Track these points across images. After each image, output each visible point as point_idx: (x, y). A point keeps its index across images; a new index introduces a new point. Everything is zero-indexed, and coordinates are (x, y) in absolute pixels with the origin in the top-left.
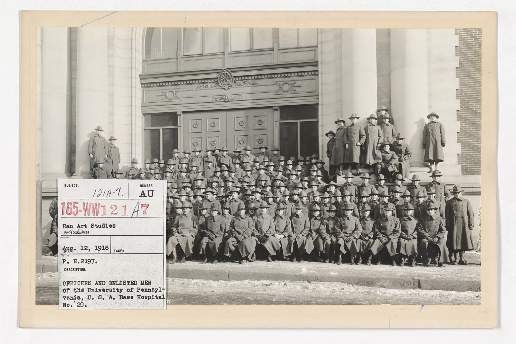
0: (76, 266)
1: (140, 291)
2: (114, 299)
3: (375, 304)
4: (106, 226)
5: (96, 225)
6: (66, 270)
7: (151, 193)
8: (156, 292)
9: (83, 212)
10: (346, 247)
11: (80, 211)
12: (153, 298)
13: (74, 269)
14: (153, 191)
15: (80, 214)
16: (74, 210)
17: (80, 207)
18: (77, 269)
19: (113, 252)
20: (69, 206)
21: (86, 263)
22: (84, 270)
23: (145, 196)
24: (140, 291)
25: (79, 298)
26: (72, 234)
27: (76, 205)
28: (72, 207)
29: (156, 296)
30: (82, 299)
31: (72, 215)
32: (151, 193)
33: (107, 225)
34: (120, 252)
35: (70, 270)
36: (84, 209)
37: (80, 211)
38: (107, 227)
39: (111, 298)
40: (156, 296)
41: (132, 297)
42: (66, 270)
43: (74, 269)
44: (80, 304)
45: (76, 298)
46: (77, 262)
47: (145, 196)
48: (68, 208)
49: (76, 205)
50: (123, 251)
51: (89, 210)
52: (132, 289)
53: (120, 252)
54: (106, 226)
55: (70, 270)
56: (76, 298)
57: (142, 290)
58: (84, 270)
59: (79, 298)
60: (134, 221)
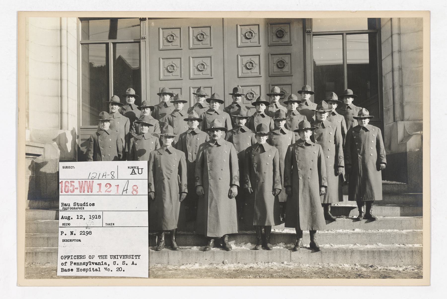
0: (72, 237)
1: (73, 264)
2: (136, 264)
3: (306, 277)
4: (86, 205)
5: (78, 204)
6: (64, 241)
7: (140, 170)
8: (86, 265)
9: (79, 190)
10: (160, 239)
11: (77, 188)
12: (90, 271)
13: (71, 240)
14: (142, 169)
15: (77, 192)
16: (71, 188)
17: (76, 184)
18: (73, 240)
19: (104, 225)
20: (67, 184)
21: (84, 234)
22: (80, 241)
23: (135, 174)
24: (73, 264)
25: (106, 264)
26: (70, 210)
27: (73, 184)
28: (69, 185)
29: (93, 269)
30: (109, 265)
31: (70, 193)
32: (140, 170)
33: (87, 203)
34: (111, 225)
35: (67, 241)
36: (80, 186)
37: (77, 188)
38: (87, 206)
39: (133, 263)
40: (93, 269)
41: (72, 270)
42: (64, 241)
43: (71, 240)
44: (119, 269)
45: (104, 263)
46: (74, 234)
47: (135, 174)
48: (66, 186)
49: (73, 184)
50: (114, 224)
51: (84, 187)
52: (66, 263)
53: (111, 225)
54: (86, 205)
55: (67, 241)
56: (104, 263)
57: (75, 264)
58: (80, 241)
59: (106, 264)
60: (113, 199)
